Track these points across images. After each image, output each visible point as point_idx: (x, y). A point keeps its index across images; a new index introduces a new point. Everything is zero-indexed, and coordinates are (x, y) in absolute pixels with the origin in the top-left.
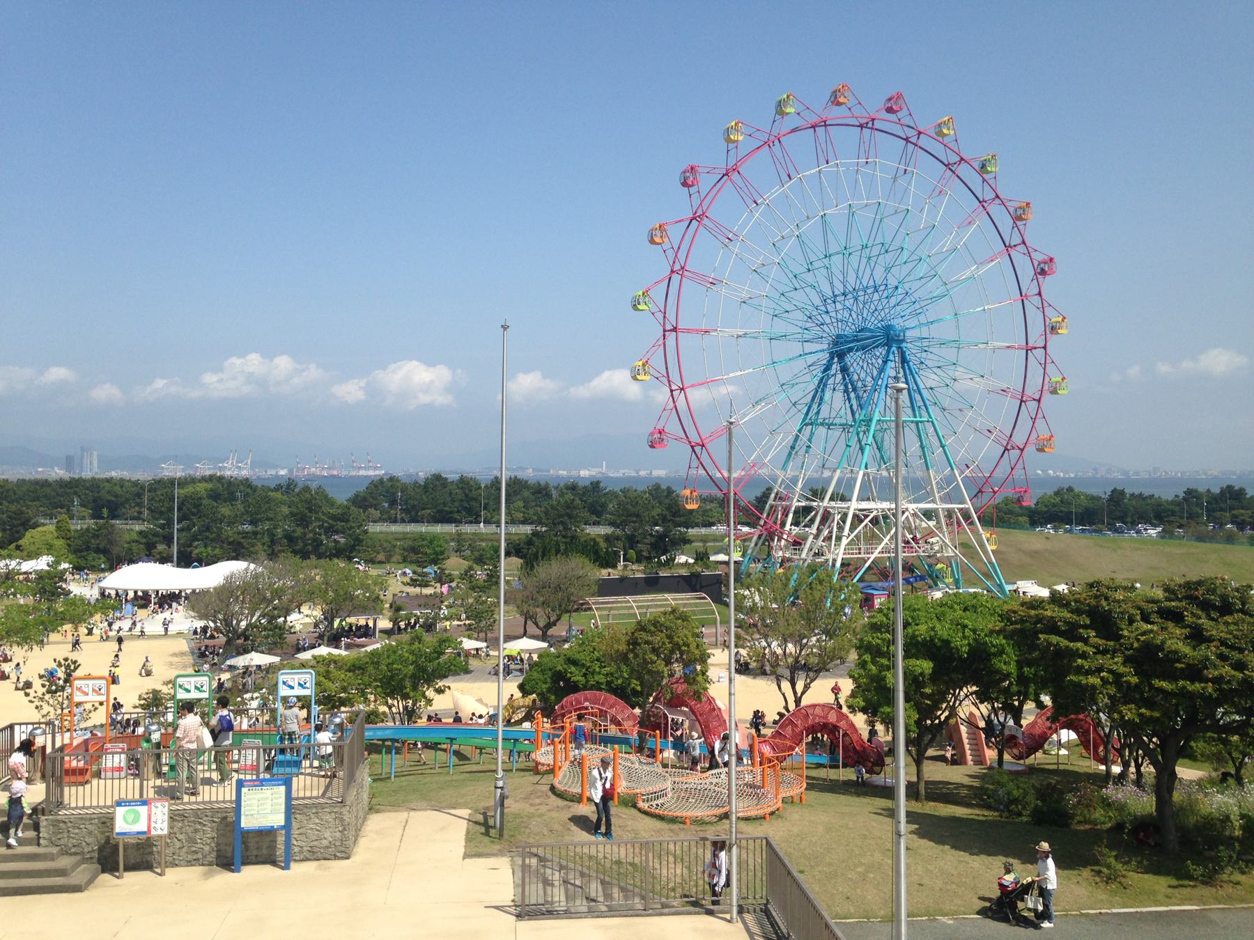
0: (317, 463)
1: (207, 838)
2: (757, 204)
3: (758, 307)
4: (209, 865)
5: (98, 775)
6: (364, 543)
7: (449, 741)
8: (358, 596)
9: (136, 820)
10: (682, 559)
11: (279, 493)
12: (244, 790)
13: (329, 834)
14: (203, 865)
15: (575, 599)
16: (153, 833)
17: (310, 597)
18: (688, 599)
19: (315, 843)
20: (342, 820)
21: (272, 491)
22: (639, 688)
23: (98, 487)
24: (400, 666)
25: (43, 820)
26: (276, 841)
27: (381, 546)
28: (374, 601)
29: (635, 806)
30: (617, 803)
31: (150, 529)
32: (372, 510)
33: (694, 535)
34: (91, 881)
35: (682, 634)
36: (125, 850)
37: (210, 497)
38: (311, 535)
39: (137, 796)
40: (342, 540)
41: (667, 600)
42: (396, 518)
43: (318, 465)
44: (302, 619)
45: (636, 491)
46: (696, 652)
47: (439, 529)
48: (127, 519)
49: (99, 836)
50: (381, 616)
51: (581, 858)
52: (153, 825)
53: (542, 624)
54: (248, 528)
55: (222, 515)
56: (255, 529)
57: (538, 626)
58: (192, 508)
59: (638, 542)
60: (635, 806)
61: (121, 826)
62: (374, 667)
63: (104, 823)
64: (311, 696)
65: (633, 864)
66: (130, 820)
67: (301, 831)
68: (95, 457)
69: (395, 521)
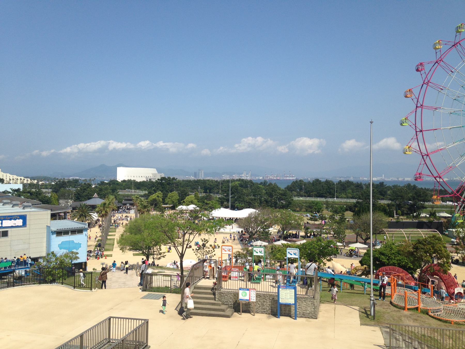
0: (272, 175)
1: (268, 304)
2: (453, 72)
3: (460, 115)
4: (268, 314)
5: (230, 278)
6: (292, 204)
7: (340, 280)
8: (293, 223)
9: (245, 296)
10: (423, 215)
11: (262, 185)
12: (280, 289)
13: (309, 309)
14: (267, 314)
15: (378, 229)
16: (251, 300)
17: (276, 223)
18: (428, 232)
19: (305, 311)
20: (314, 305)
21: (259, 185)
22: (412, 267)
23: (205, 183)
24: (313, 250)
25: (217, 292)
26: (291, 309)
27: (298, 205)
28: (298, 225)
29: (427, 314)
30: (419, 312)
31: (222, 197)
32: (294, 192)
33: (427, 205)
34: (232, 314)
35: (438, 246)
36: (242, 305)
37: (240, 186)
38: (273, 200)
39: (245, 287)
40: (284, 203)
41: (419, 231)
42: (302, 195)
43: (273, 176)
44: (274, 230)
45: (399, 186)
46: (445, 254)
47: (319, 199)
48: (214, 193)
49: (234, 299)
50: (301, 231)
51: (408, 332)
52: (251, 298)
53: (364, 238)
54: (253, 198)
55: (244, 193)
56: (255, 198)
57: (362, 239)
58: (235, 190)
59: (402, 207)
60: (427, 314)
61: (241, 297)
62: (304, 249)
63: (235, 295)
64: (298, 258)
65: (430, 337)
66: (244, 295)
67: (299, 306)
68: (203, 172)
69: (302, 196)
